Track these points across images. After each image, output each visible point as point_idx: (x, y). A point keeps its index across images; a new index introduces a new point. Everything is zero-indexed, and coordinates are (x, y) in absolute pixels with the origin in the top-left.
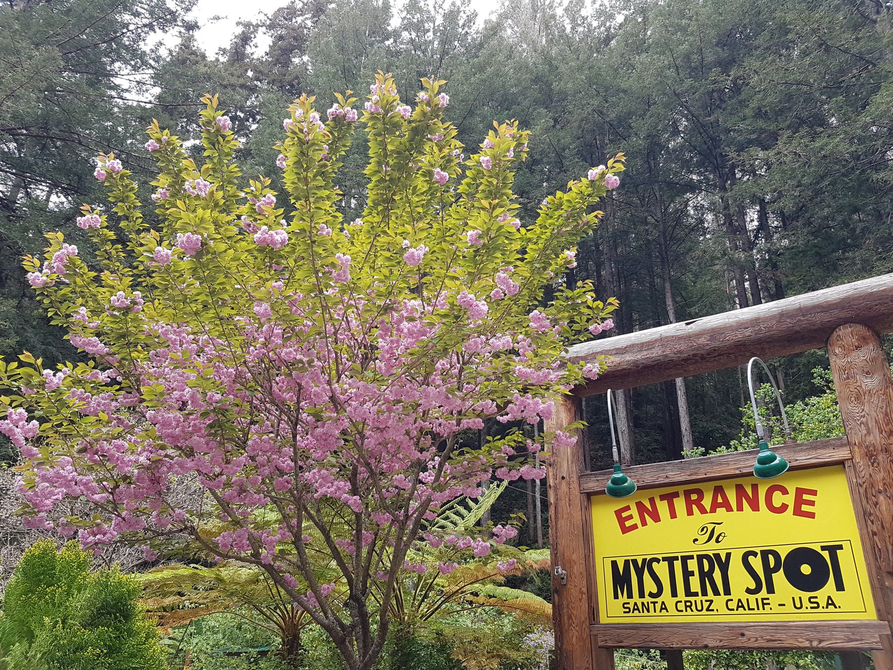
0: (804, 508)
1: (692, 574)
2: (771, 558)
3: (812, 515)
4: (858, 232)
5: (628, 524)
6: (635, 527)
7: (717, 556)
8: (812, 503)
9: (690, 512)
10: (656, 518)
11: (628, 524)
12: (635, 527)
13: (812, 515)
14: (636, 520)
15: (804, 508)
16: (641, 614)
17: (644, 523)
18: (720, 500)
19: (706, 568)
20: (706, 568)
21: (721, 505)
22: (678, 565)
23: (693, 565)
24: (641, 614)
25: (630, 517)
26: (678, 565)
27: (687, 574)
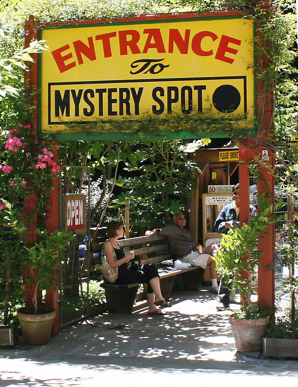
0: (227, 55)
1: (115, 101)
2: (173, 92)
3: (231, 61)
4: (17, 209)
5: (67, 63)
6: (73, 65)
7: (133, 89)
8: (234, 52)
9: (123, 52)
10: (92, 56)
11: (67, 63)
12: (73, 65)
13: (231, 61)
14: (74, 59)
15: (227, 55)
16: (70, 87)
17: (81, 62)
18: (153, 41)
19: (125, 97)
20: (125, 97)
21: (153, 46)
22: (105, 95)
23: (115, 96)
24: (70, 87)
25: (70, 56)
26: (105, 95)
27: (111, 101)
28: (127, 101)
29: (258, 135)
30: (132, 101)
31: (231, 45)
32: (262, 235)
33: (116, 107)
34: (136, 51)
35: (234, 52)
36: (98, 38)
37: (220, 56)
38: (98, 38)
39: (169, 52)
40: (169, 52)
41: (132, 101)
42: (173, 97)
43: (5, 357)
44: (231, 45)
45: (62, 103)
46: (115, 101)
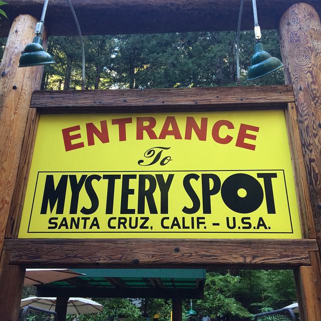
1: (132, 192)
3: (252, 147)
9: (140, 137)
12: (81, 145)
13: (252, 147)
14: (84, 139)
17: (91, 142)
19: (147, 187)
20: (147, 187)
22: (118, 183)
23: (134, 184)
26: (118, 183)
27: (126, 192)
28: (150, 194)
29: (3, 174)
30: (157, 195)
31: (248, 132)
32: (216, 310)
33: (133, 202)
34: (152, 136)
35: (254, 138)
36: (82, 218)
37: (240, 143)
38: (82, 218)
39: (186, 138)
40: (186, 138)
41: (157, 195)
42: (211, 187)
43: (50, 283)
44: (248, 132)
45: (53, 195)
46: (132, 192)
